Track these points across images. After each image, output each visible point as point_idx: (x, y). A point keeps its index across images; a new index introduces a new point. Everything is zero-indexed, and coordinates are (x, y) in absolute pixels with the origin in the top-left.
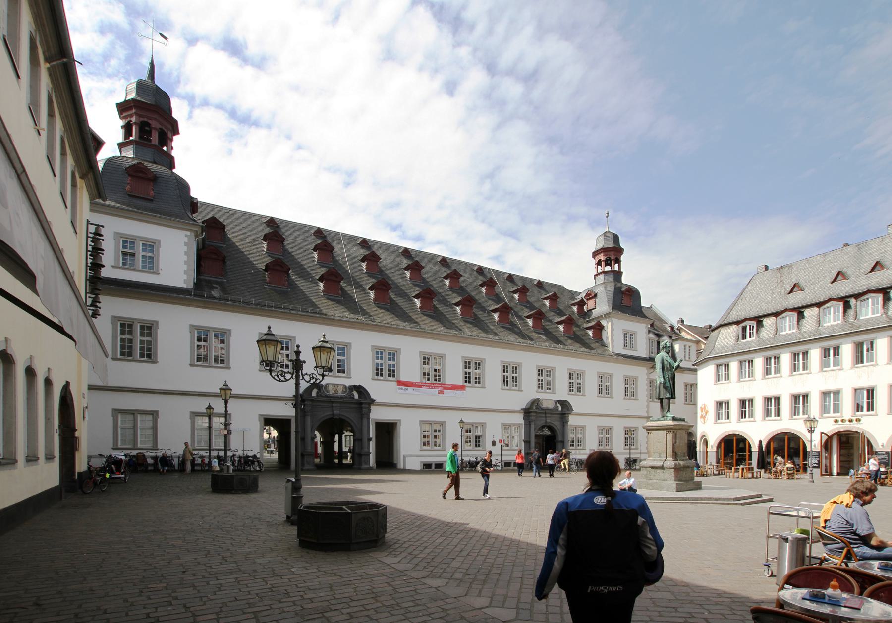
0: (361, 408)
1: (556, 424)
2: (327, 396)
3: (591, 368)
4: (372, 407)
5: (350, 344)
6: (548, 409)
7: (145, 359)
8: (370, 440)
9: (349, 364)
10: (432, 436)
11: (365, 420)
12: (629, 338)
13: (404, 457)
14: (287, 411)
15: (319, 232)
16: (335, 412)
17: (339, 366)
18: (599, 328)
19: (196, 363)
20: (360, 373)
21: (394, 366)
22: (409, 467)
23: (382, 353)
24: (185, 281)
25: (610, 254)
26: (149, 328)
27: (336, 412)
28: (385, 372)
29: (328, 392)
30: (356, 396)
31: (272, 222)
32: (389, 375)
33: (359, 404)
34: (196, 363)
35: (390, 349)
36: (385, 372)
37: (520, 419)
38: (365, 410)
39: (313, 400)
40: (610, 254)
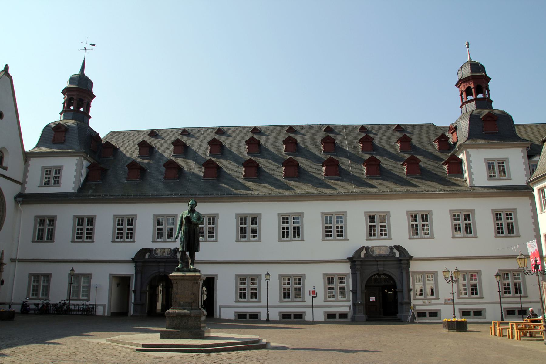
0: (401, 264)
1: (393, 272)
2: (155, 258)
3: (441, 210)
4: (411, 263)
5: (346, 212)
6: (380, 256)
7: (49, 240)
8: (134, 292)
9: (346, 228)
10: (248, 288)
11: (404, 274)
12: (497, 168)
13: (220, 307)
14: (129, 270)
15: (399, 128)
16: (160, 270)
17: (417, 230)
18: (456, 166)
19: (76, 240)
20: (399, 235)
21: (342, 227)
22: (223, 317)
23: (330, 218)
24: (74, 188)
25: (476, 82)
26: (297, 218)
27: (381, 268)
28: (334, 233)
29: (157, 254)
30: (397, 255)
31: (363, 128)
32: (338, 236)
33: (399, 260)
34: (76, 240)
35: (336, 213)
36: (334, 233)
37: (345, 269)
38: (404, 266)
39: (362, 261)
40: (476, 82)
